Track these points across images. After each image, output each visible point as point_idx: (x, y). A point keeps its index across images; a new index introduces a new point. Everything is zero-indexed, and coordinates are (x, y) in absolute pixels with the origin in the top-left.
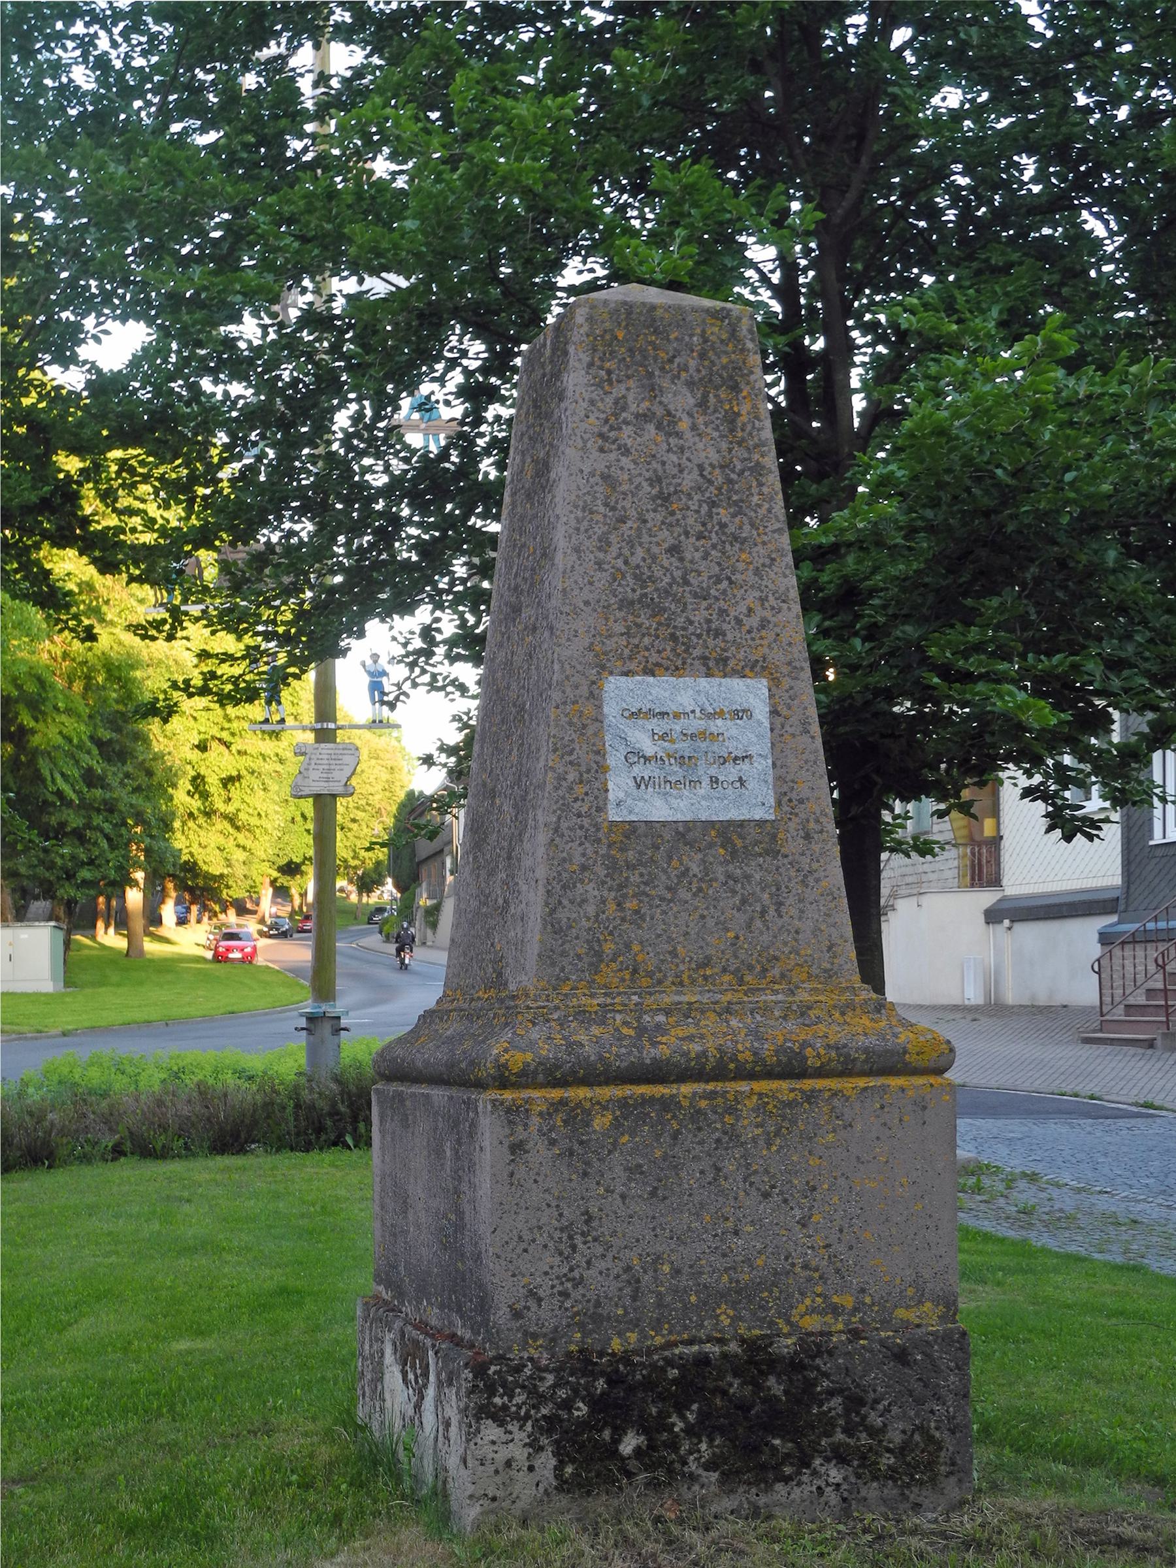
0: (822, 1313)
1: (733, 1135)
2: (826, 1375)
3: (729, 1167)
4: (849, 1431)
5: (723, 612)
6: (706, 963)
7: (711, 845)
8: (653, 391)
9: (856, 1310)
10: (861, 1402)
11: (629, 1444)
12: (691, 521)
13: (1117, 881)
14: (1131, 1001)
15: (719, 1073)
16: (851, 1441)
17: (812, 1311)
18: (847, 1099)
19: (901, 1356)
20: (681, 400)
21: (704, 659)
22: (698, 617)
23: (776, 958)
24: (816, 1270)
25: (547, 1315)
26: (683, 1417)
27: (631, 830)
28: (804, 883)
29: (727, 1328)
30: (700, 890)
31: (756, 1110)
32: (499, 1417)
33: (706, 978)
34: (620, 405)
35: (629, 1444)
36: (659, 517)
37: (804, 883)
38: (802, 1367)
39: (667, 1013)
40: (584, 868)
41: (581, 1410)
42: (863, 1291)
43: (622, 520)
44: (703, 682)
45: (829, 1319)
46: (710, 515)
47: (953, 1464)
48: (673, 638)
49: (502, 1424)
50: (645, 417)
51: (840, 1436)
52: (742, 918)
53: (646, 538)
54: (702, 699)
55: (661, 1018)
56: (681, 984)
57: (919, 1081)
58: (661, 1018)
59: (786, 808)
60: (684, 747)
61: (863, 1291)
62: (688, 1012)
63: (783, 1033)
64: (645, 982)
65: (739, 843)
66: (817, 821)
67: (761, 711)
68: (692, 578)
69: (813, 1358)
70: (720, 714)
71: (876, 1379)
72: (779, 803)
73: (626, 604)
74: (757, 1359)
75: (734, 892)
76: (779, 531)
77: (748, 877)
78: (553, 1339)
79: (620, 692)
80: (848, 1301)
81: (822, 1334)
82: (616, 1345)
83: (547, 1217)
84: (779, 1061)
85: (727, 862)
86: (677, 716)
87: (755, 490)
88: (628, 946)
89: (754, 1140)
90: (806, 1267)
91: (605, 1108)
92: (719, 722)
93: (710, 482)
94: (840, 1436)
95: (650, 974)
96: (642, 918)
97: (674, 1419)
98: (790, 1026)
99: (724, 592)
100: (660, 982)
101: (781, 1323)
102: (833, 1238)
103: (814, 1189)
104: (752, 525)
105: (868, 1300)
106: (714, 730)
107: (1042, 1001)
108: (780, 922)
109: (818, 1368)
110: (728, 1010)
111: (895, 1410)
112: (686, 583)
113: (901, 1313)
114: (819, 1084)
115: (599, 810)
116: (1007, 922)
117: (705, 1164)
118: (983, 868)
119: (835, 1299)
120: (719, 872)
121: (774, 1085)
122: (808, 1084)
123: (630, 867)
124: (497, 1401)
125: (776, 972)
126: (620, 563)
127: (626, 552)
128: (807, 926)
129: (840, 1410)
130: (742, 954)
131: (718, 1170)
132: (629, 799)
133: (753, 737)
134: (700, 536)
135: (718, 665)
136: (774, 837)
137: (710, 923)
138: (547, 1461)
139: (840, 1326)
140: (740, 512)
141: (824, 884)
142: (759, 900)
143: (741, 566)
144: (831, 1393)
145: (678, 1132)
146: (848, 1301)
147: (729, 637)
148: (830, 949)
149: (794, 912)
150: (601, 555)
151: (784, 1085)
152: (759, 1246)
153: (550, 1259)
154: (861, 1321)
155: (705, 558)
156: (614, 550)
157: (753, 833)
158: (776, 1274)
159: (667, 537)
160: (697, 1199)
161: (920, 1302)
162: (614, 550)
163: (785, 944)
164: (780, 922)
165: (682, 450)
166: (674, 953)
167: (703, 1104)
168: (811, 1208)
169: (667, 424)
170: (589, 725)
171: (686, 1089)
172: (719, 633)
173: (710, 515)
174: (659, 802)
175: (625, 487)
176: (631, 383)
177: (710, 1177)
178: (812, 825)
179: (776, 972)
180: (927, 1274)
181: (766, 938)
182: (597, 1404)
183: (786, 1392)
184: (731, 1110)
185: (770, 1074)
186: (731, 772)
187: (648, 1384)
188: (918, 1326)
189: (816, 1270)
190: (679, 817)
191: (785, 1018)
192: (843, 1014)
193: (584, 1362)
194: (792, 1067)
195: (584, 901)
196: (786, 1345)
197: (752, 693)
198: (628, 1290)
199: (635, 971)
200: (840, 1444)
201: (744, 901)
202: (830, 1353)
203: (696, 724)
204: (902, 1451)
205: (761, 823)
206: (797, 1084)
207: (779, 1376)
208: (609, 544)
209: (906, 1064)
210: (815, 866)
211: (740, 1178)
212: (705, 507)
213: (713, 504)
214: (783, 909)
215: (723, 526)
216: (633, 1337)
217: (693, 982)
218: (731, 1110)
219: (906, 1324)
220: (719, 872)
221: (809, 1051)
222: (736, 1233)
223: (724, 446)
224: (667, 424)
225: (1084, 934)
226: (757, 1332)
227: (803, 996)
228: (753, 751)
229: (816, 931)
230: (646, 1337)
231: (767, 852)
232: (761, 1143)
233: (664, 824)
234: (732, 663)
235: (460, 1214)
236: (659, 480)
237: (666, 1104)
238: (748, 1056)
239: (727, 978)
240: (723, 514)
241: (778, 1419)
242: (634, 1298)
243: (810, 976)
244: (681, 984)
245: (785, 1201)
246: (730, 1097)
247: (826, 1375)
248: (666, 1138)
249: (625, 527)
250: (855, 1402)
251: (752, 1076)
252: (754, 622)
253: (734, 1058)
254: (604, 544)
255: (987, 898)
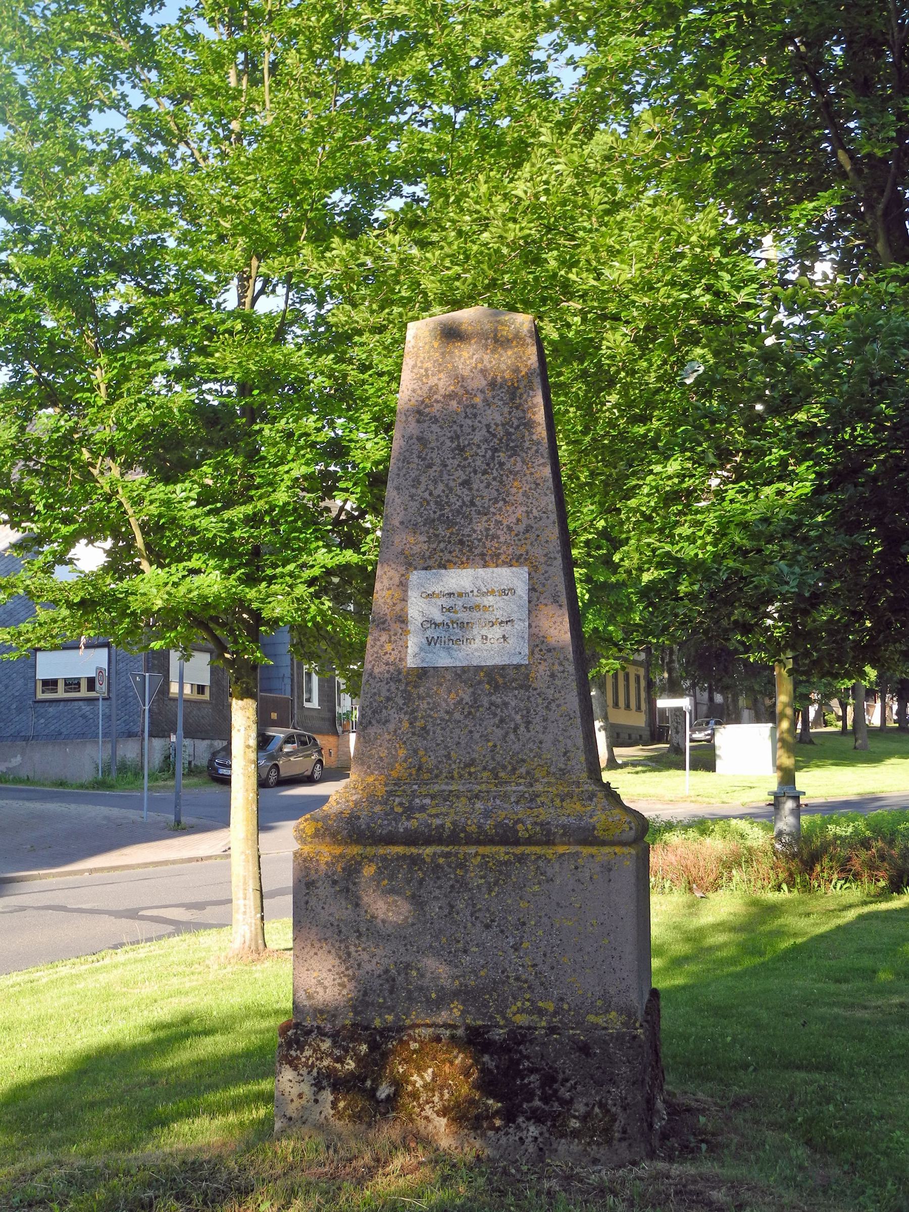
0: (530, 1013)
1: (462, 884)
2: (528, 1058)
3: (461, 906)
4: (545, 1099)
5: (498, 523)
6: (472, 763)
7: (480, 683)
9: (556, 1013)
10: (554, 1080)
12: (478, 463)
15: (453, 839)
16: (547, 1108)
17: (521, 1011)
18: (549, 861)
19: (584, 1049)
21: (483, 555)
22: (479, 527)
23: (524, 761)
24: (526, 981)
26: (422, 1077)
28: (548, 708)
30: (470, 713)
31: (480, 866)
33: (470, 774)
36: (456, 462)
37: (548, 708)
38: (509, 1051)
39: (433, 797)
40: (388, 699)
42: (562, 999)
43: (430, 466)
44: (481, 571)
45: (535, 1017)
46: (493, 458)
47: (624, 1132)
48: (461, 542)
49: (295, 1068)
51: (537, 1103)
52: (499, 732)
53: (445, 477)
54: (479, 583)
55: (427, 801)
56: (452, 778)
57: (606, 850)
58: (427, 801)
59: (537, 656)
61: (562, 999)
62: (446, 797)
63: (506, 812)
64: (426, 776)
65: (501, 681)
66: (561, 664)
67: (522, 589)
68: (477, 501)
69: (519, 1044)
70: (492, 592)
71: (565, 1064)
72: (532, 653)
73: (429, 522)
75: (495, 715)
76: (544, 465)
77: (506, 704)
80: (551, 1007)
81: (529, 1028)
82: (377, 1023)
84: (497, 833)
85: (490, 694)
86: (460, 595)
87: (527, 438)
88: (416, 751)
89: (479, 887)
90: (517, 979)
91: (371, 861)
92: (491, 598)
93: (494, 436)
94: (537, 1103)
95: (430, 771)
96: (427, 733)
97: (415, 1077)
98: (518, 808)
99: (500, 509)
100: (437, 776)
101: (498, 1017)
102: (539, 960)
103: (524, 924)
104: (523, 462)
105: (566, 1007)
106: (487, 604)
108: (528, 735)
109: (520, 1052)
110: (477, 797)
111: (579, 1087)
112: (472, 504)
113: (591, 1018)
114: (528, 850)
115: (401, 660)
117: (443, 902)
119: (540, 1004)
120: (485, 702)
121: (494, 849)
122: (519, 850)
123: (420, 697)
124: (293, 1053)
125: (523, 770)
126: (426, 495)
127: (431, 487)
128: (548, 738)
129: (537, 1084)
130: (498, 758)
131: (452, 907)
134: (485, 472)
136: (527, 676)
137: (476, 736)
139: (544, 1024)
140: (515, 454)
141: (563, 708)
142: (513, 720)
143: (514, 490)
144: (532, 1071)
145: (423, 879)
146: (551, 1007)
147: (502, 539)
148: (565, 754)
149: (539, 728)
150: (413, 491)
151: (502, 849)
152: (482, 962)
154: (561, 1021)
155: (487, 487)
156: (423, 487)
157: (512, 673)
158: (495, 982)
159: (461, 475)
160: (437, 926)
161: (607, 1012)
162: (423, 487)
163: (531, 750)
164: (528, 735)
165: (475, 416)
166: (448, 757)
167: (441, 861)
168: (522, 937)
171: (429, 850)
172: (495, 537)
173: (493, 458)
174: (443, 654)
175: (433, 444)
176: (442, 375)
177: (446, 911)
178: (557, 667)
179: (523, 770)
180: (612, 990)
181: (516, 747)
183: (497, 1067)
184: (462, 866)
185: (490, 841)
188: (606, 1028)
189: (526, 981)
190: (458, 664)
191: (517, 803)
192: (562, 801)
194: (507, 836)
195: (387, 721)
196: (498, 1034)
198: (386, 986)
199: (420, 769)
200: (538, 1109)
201: (502, 721)
202: (531, 1042)
205: (518, 667)
206: (511, 849)
207: (491, 1055)
208: (419, 483)
209: (596, 837)
210: (557, 695)
211: (468, 913)
212: (490, 453)
213: (495, 450)
214: (531, 727)
215: (501, 464)
216: (390, 1018)
217: (461, 777)
218: (462, 866)
219: (596, 1026)
220: (485, 702)
221: (520, 827)
222: (465, 951)
223: (506, 410)
226: (480, 1023)
227: (539, 788)
228: (514, 617)
229: (556, 742)
230: (399, 1019)
231: (521, 687)
232: (484, 889)
233: (447, 669)
234: (503, 557)
236: (458, 437)
237: (415, 861)
238: (474, 828)
239: (485, 774)
240: (502, 456)
242: (391, 992)
243: (548, 773)
244: (452, 778)
245: (502, 931)
246: (461, 856)
247: (528, 1058)
248: (414, 883)
249: (431, 471)
250: (549, 1079)
251: (478, 843)
252: (521, 527)
253: (464, 830)
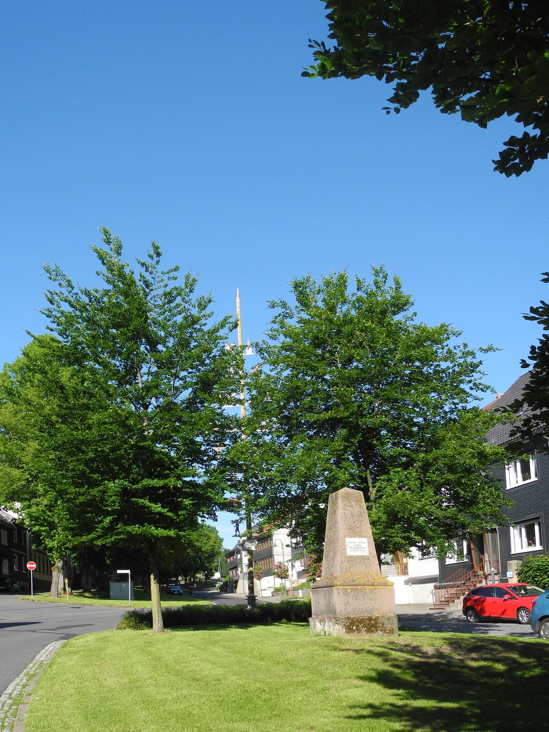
1: (366, 593)
8: (350, 502)
11: (354, 628)
13: (438, 573)
14: (440, 600)
19: (389, 619)
20: (354, 503)
25: (343, 613)
27: (350, 556)
29: (366, 615)
32: (338, 624)
34: (346, 504)
35: (354, 628)
41: (348, 624)
50: (349, 506)
60: (357, 546)
74: (370, 619)
78: (344, 615)
79: (348, 540)
83: (343, 601)
107: (420, 602)
116: (410, 584)
118: (404, 571)
128: (374, 568)
132: (350, 552)
133: (366, 545)
135: (360, 536)
138: (344, 629)
153: (343, 606)
169: (352, 507)
170: (344, 544)
182: (350, 623)
186: (363, 550)
187: (356, 621)
193: (348, 618)
196: (374, 618)
197: (365, 540)
203: (358, 544)
204: (389, 630)
224: (352, 507)
225: (431, 586)
235: (330, 602)
237: (357, 589)
241: (373, 626)
254: (345, 521)
255: (406, 578)
